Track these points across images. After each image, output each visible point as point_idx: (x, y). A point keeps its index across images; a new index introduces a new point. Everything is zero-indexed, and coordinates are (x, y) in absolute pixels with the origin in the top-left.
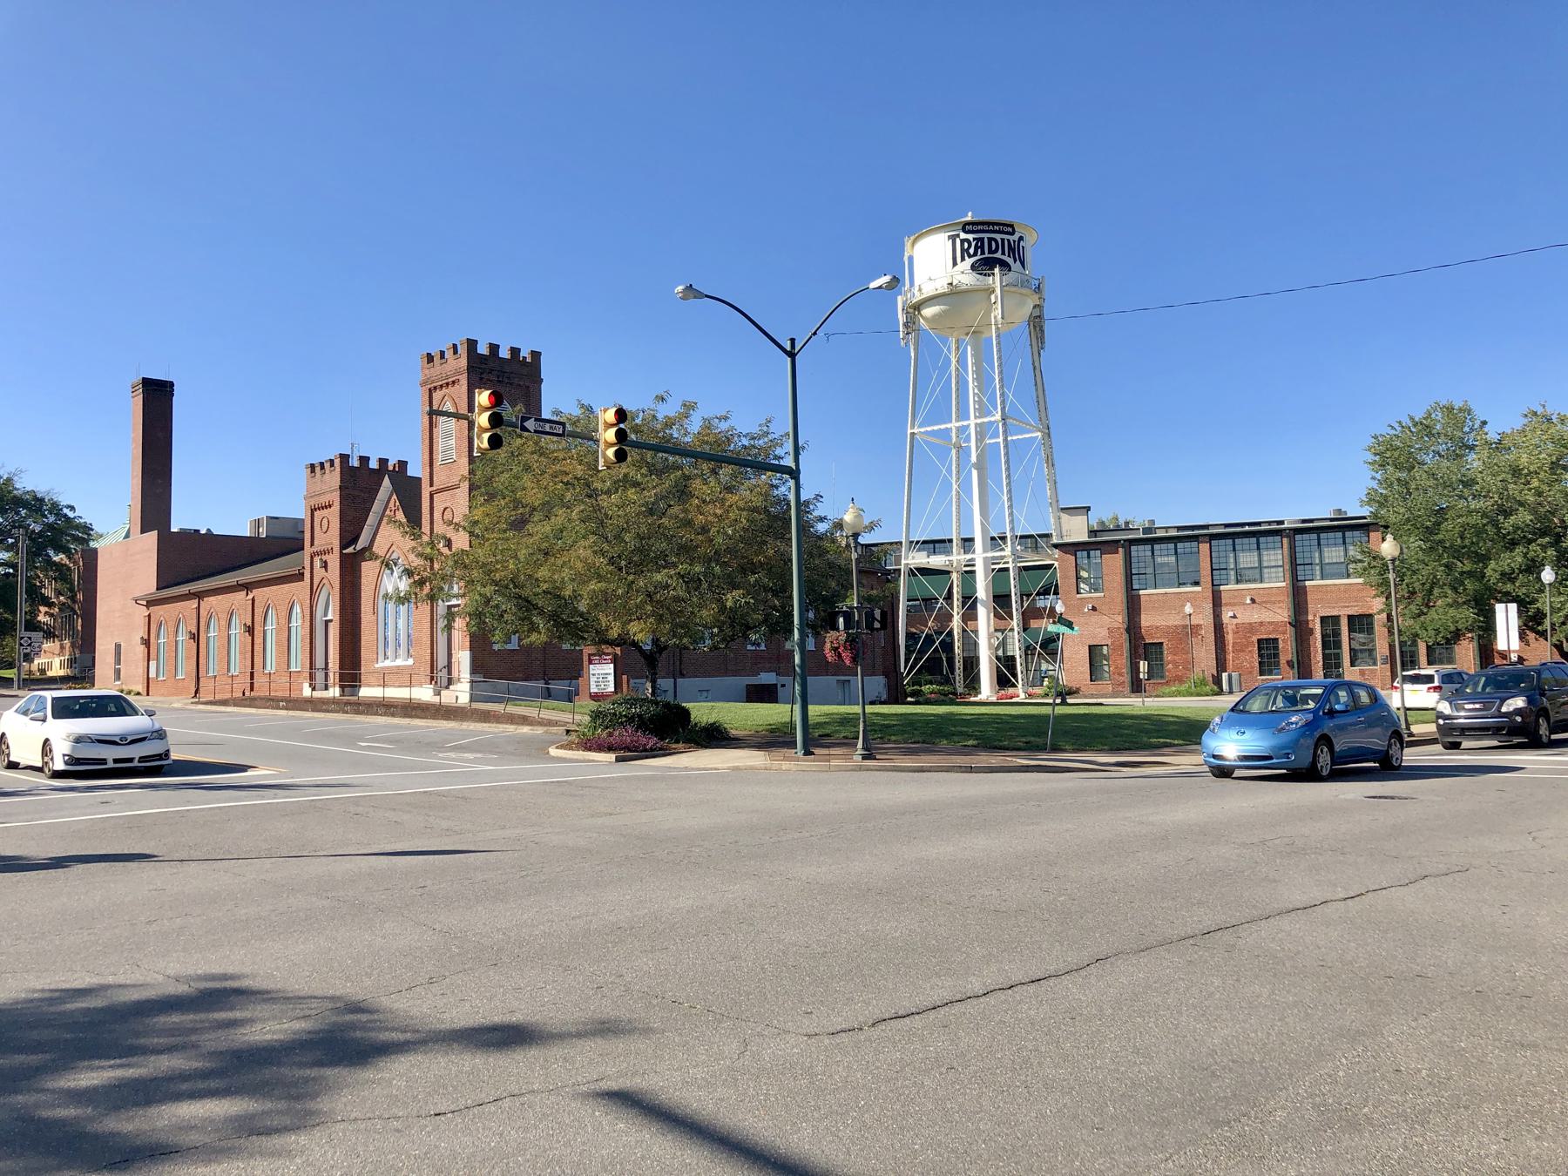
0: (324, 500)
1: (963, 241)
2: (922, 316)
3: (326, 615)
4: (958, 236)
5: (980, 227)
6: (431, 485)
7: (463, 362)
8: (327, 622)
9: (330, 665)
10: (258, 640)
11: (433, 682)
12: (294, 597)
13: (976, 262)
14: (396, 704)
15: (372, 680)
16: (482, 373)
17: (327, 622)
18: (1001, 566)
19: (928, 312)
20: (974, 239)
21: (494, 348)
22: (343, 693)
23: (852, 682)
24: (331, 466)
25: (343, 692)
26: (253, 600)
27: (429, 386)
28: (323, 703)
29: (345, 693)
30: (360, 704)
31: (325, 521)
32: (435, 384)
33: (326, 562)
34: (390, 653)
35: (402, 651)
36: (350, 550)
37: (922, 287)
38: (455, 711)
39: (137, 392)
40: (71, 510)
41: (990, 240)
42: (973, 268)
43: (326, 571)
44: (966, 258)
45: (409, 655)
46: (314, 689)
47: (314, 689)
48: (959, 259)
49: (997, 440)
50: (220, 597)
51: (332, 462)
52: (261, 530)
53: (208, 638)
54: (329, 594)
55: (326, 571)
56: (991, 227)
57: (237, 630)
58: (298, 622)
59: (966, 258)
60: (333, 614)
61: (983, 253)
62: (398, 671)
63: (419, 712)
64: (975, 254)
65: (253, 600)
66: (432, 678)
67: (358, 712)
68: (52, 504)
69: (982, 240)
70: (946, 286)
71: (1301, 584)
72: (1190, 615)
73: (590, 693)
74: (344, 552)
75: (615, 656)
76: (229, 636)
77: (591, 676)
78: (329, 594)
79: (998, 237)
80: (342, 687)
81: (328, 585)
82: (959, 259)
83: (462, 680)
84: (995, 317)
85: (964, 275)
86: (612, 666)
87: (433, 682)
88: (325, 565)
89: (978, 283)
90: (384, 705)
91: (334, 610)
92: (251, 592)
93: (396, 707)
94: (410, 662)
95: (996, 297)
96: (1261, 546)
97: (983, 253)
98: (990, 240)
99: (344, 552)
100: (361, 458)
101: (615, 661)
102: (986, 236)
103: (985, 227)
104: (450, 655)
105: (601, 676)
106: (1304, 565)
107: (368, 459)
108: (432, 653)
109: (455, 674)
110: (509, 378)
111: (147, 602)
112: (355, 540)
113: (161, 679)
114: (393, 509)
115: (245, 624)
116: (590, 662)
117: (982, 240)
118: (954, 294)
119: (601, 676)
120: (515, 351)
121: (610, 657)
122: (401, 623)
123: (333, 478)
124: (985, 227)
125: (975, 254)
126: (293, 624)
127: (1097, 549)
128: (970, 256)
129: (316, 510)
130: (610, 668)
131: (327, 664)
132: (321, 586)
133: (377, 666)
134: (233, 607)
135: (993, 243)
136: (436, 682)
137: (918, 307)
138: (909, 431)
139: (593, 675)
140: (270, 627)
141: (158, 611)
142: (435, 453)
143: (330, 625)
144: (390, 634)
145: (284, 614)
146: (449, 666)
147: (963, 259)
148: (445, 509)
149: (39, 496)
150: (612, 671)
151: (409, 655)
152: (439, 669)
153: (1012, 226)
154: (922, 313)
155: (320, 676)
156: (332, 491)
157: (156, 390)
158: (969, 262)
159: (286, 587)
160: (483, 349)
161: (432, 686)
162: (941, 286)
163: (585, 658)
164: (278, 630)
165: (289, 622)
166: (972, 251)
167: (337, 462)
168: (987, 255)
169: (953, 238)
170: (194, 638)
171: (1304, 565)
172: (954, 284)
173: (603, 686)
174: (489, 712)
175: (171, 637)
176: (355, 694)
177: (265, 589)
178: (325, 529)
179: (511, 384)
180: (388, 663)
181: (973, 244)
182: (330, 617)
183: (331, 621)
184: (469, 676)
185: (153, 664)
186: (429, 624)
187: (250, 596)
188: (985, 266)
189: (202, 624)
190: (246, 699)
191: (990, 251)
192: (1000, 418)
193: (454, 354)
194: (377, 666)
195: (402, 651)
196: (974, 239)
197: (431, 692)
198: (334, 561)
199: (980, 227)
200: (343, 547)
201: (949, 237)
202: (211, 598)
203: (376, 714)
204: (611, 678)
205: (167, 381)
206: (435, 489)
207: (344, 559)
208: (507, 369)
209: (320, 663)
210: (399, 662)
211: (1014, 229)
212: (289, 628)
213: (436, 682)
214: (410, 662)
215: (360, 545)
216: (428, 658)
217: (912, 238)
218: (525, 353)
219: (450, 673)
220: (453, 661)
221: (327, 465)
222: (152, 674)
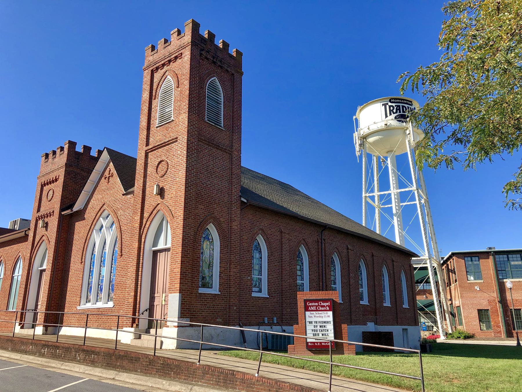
1: (390, 107)
2: (367, 141)
4: (387, 104)
5: (398, 101)
6: (147, 144)
7: (187, 38)
8: (42, 271)
11: (135, 325)
12: (20, 254)
13: (397, 116)
14: (98, 350)
15: (73, 320)
19: (371, 140)
20: (395, 106)
21: (212, 36)
22: (45, 332)
25: (46, 330)
27: (151, 69)
29: (48, 332)
30: (57, 347)
31: (51, 193)
33: (47, 223)
34: (92, 297)
35: (104, 295)
36: (68, 212)
37: (370, 127)
38: (178, 366)
41: (403, 107)
42: (395, 118)
44: (392, 114)
45: (109, 299)
46: (22, 328)
47: (22, 328)
48: (388, 114)
52: (16, 227)
54: (47, 249)
56: (403, 101)
59: (392, 114)
60: (47, 265)
61: (400, 112)
62: (100, 313)
63: (125, 363)
64: (396, 112)
67: (55, 357)
69: (399, 106)
70: (384, 126)
71: (501, 280)
72: (511, 289)
73: (307, 343)
75: (333, 302)
77: (308, 324)
78: (47, 249)
79: (406, 106)
80: (46, 327)
82: (388, 114)
83: (168, 324)
85: (391, 120)
86: (330, 313)
87: (135, 325)
89: (400, 125)
90: (84, 351)
91: (48, 261)
93: (97, 354)
94: (111, 304)
95: (410, 131)
96: (510, 259)
97: (400, 112)
99: (63, 213)
100: (85, 147)
101: (334, 307)
103: (400, 101)
104: (152, 298)
105: (319, 325)
106: (502, 270)
108: (136, 296)
110: (221, 62)
112: (71, 206)
114: (108, 176)
116: (307, 309)
118: (387, 130)
119: (319, 325)
121: (328, 304)
122: (105, 271)
123: (62, 159)
124: (400, 101)
126: (16, 273)
127: (469, 257)
128: (394, 113)
130: (329, 316)
131: (37, 305)
132: (40, 242)
133: (79, 308)
135: (404, 108)
136: (137, 325)
137: (364, 138)
139: (310, 322)
142: (152, 119)
143: (44, 274)
144: (94, 280)
145: (10, 267)
147: (390, 114)
148: (160, 163)
150: (331, 319)
151: (109, 299)
152: (141, 312)
153: (411, 102)
154: (367, 140)
155: (29, 316)
156: (58, 169)
158: (393, 116)
159: (15, 247)
161: (132, 330)
162: (381, 125)
163: (301, 305)
166: (395, 111)
167: (66, 147)
168: (402, 113)
169: (385, 105)
171: (502, 270)
172: (388, 125)
173: (321, 335)
176: (56, 332)
178: (49, 198)
179: (221, 67)
180: (89, 305)
181: (395, 108)
182: (44, 267)
183: (44, 270)
184: (177, 320)
186: (135, 268)
188: (402, 118)
191: (403, 112)
193: (178, 36)
194: (79, 308)
195: (104, 295)
196: (395, 106)
197: (132, 336)
198: (54, 222)
199: (398, 101)
200: (62, 209)
201: (383, 105)
203: (74, 360)
206: (150, 147)
208: (219, 54)
209: (31, 304)
210: (100, 305)
212: (12, 278)
213: (137, 325)
214: (111, 304)
215: (76, 208)
216: (131, 300)
219: (151, 314)
220: (155, 304)
221: (58, 151)
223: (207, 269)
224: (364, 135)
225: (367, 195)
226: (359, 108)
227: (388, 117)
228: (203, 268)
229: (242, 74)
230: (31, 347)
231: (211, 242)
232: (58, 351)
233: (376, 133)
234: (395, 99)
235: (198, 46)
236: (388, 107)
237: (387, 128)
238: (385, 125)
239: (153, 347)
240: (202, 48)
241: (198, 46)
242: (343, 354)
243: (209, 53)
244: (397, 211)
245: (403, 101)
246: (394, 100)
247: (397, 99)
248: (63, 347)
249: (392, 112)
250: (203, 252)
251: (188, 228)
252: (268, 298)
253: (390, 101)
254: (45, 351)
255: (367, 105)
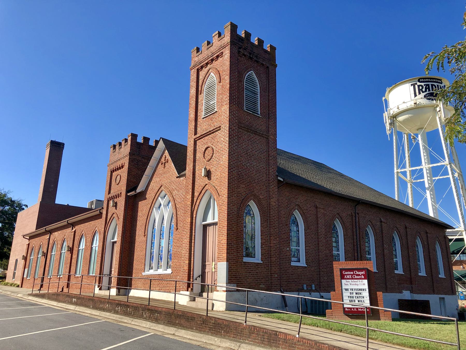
0: (119, 164)
1: (419, 86)
3: (113, 239)
4: (416, 84)
5: (427, 80)
6: (195, 134)
7: (227, 38)
8: (114, 243)
9: (113, 272)
10: (75, 256)
11: (190, 289)
14: (160, 309)
15: (140, 284)
16: (240, 48)
17: (114, 243)
18: (457, 237)
19: (401, 118)
20: (424, 85)
22: (118, 294)
23: (445, 299)
24: (125, 142)
25: (119, 292)
26: (75, 232)
27: (197, 68)
28: (101, 302)
29: (121, 293)
30: (128, 306)
31: (119, 177)
32: (202, 64)
33: (116, 203)
34: (154, 264)
39: (48, 147)
40: (26, 207)
41: (432, 85)
42: (425, 96)
43: (116, 209)
44: (421, 93)
45: (168, 266)
46: (100, 289)
48: (417, 93)
49: (448, 176)
50: (59, 232)
51: (126, 140)
52: (93, 206)
53: (51, 255)
55: (116, 209)
57: (65, 250)
58: (97, 245)
59: (421, 93)
61: (429, 90)
62: (161, 278)
64: (426, 91)
65: (75, 232)
66: (189, 285)
68: (18, 204)
69: (428, 85)
70: (413, 105)
73: (344, 308)
74: (128, 194)
76: (61, 254)
77: (344, 291)
78: (117, 225)
79: (436, 84)
80: (119, 289)
81: (116, 218)
82: (417, 93)
83: (218, 288)
84: (440, 118)
85: (421, 99)
86: (366, 281)
87: (190, 289)
88: (116, 205)
89: (430, 103)
90: (149, 310)
91: (118, 234)
92: (75, 228)
93: (160, 313)
94: (169, 271)
97: (429, 90)
98: (432, 85)
99: (128, 194)
101: (369, 276)
102: (430, 83)
103: (429, 80)
104: (204, 266)
105: (355, 292)
107: (149, 139)
108: (190, 264)
109: (209, 281)
110: (257, 57)
111: (30, 237)
112: (135, 188)
113: (29, 278)
115: (68, 246)
116: (343, 277)
117: (428, 85)
118: (417, 108)
120: (261, 42)
121: (363, 273)
122: (164, 243)
123: (126, 149)
124: (429, 80)
125: (426, 91)
128: (423, 92)
129: (114, 172)
130: (364, 284)
131: (111, 271)
132: (112, 218)
133: (143, 274)
134: (65, 237)
136: (192, 289)
138: (395, 171)
139: (346, 290)
140: (82, 246)
141: (36, 242)
142: (199, 111)
143: (115, 245)
146: (203, 276)
147: (420, 93)
149: (13, 200)
150: (366, 287)
151: (168, 266)
152: (194, 278)
153: (441, 80)
155: (105, 280)
156: (124, 158)
157: (56, 146)
158: (423, 95)
159: (92, 223)
160: (140, 140)
161: (188, 293)
163: (337, 273)
164: (86, 249)
165: (92, 244)
166: (424, 90)
167: (129, 139)
168: (431, 92)
169: (414, 85)
170: (45, 256)
172: (417, 104)
174: (276, 333)
175: (36, 255)
176: (127, 294)
177: (82, 225)
179: (257, 62)
180: (152, 272)
181: (424, 87)
182: (115, 240)
183: (115, 242)
184: (225, 285)
185: (26, 270)
187: (74, 230)
188: (431, 96)
189: (50, 247)
190: (63, 295)
192: (448, 163)
194: (143, 274)
196: (424, 85)
198: (121, 202)
199: (427, 80)
200: (128, 191)
201: (412, 85)
202: (56, 233)
204: (366, 294)
205: (61, 143)
206: (198, 135)
207: (128, 198)
209: (106, 270)
210: (160, 271)
211: (442, 81)
213: (192, 289)
214: (169, 271)
215: (139, 190)
217: (390, 88)
218: (267, 47)
219: (203, 280)
220: (206, 271)
222: (25, 276)
223: (250, 241)
224: (394, 114)
225: (399, 171)
226: (388, 90)
227: (417, 96)
228: (247, 240)
229: (276, 66)
230: (108, 305)
231: (253, 217)
232: (128, 309)
233: (406, 112)
234: (423, 79)
235: (236, 45)
236: (416, 86)
237: (417, 107)
238: (414, 103)
239: (206, 308)
240: (240, 46)
241: (236, 45)
242: (379, 319)
243: (246, 50)
244: (430, 185)
245: (432, 80)
246: (422, 80)
247: (426, 78)
248: (132, 307)
249: (421, 92)
250: (245, 226)
251: (231, 204)
252: (306, 267)
253: (419, 81)
254: (118, 309)
255: (395, 86)
